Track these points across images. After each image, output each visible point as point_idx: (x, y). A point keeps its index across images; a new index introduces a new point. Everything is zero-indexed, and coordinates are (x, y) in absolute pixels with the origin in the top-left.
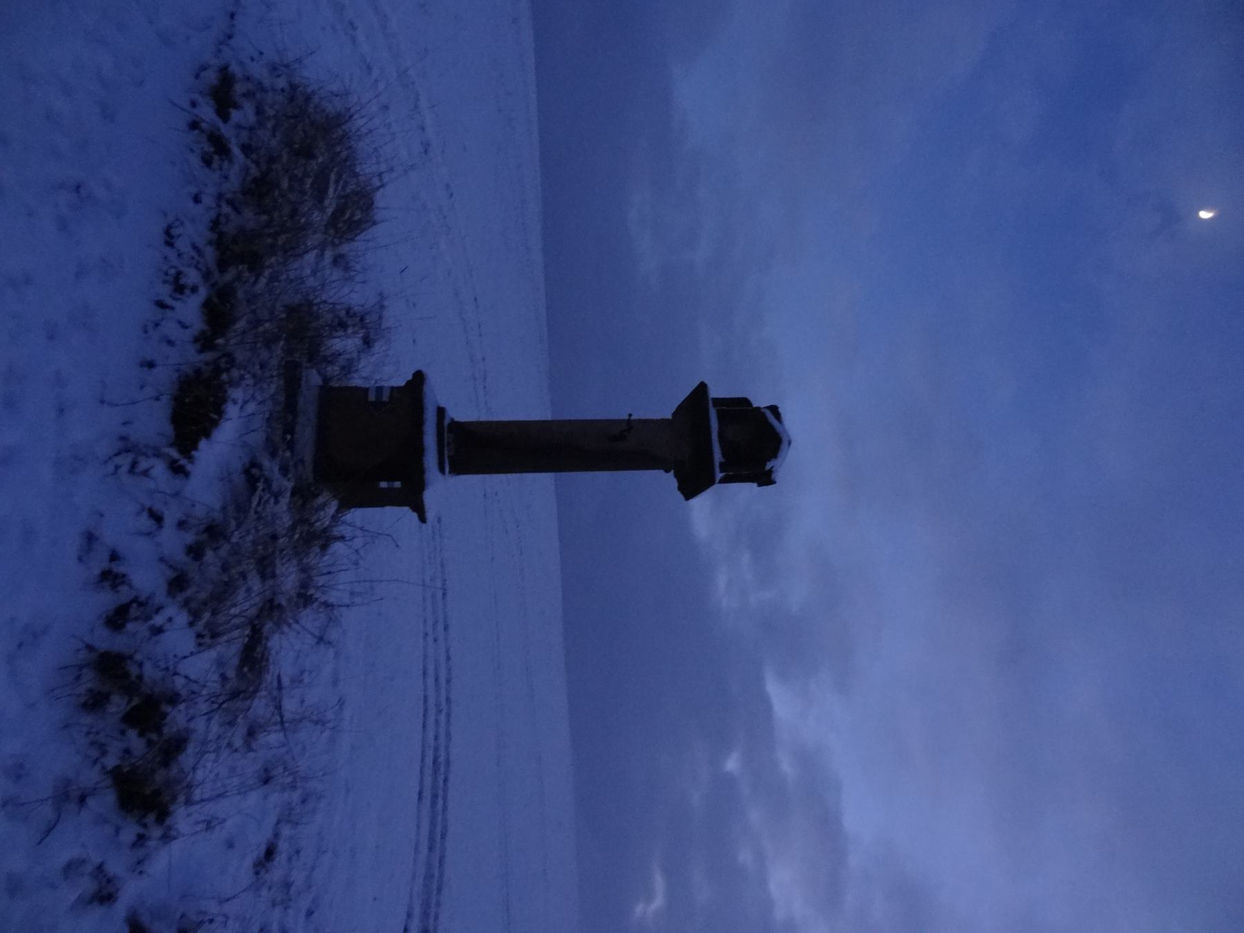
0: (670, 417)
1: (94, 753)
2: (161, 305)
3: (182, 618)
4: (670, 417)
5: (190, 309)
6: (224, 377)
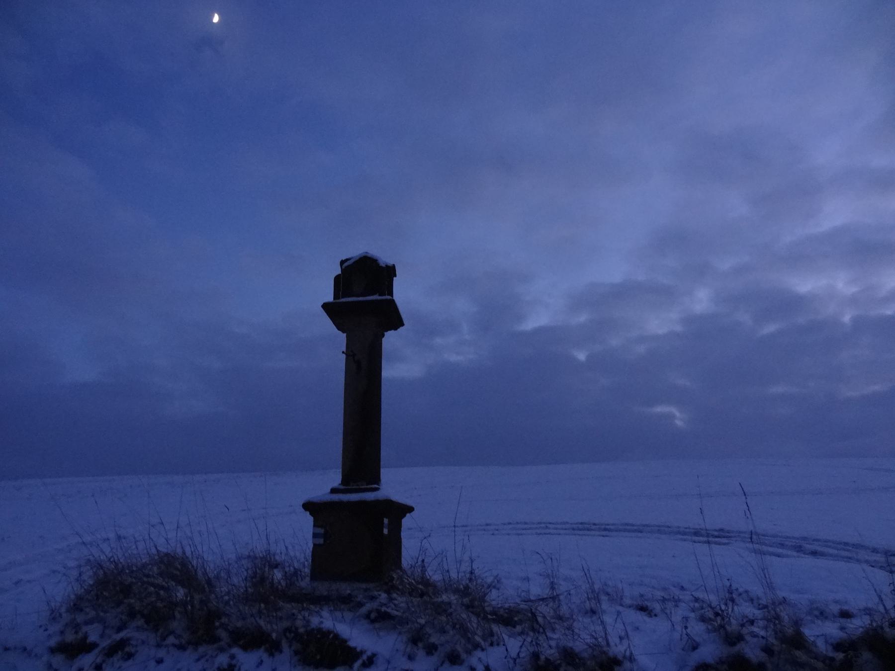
0: (345, 335)
3: (479, 653)
4: (345, 335)
6: (301, 630)
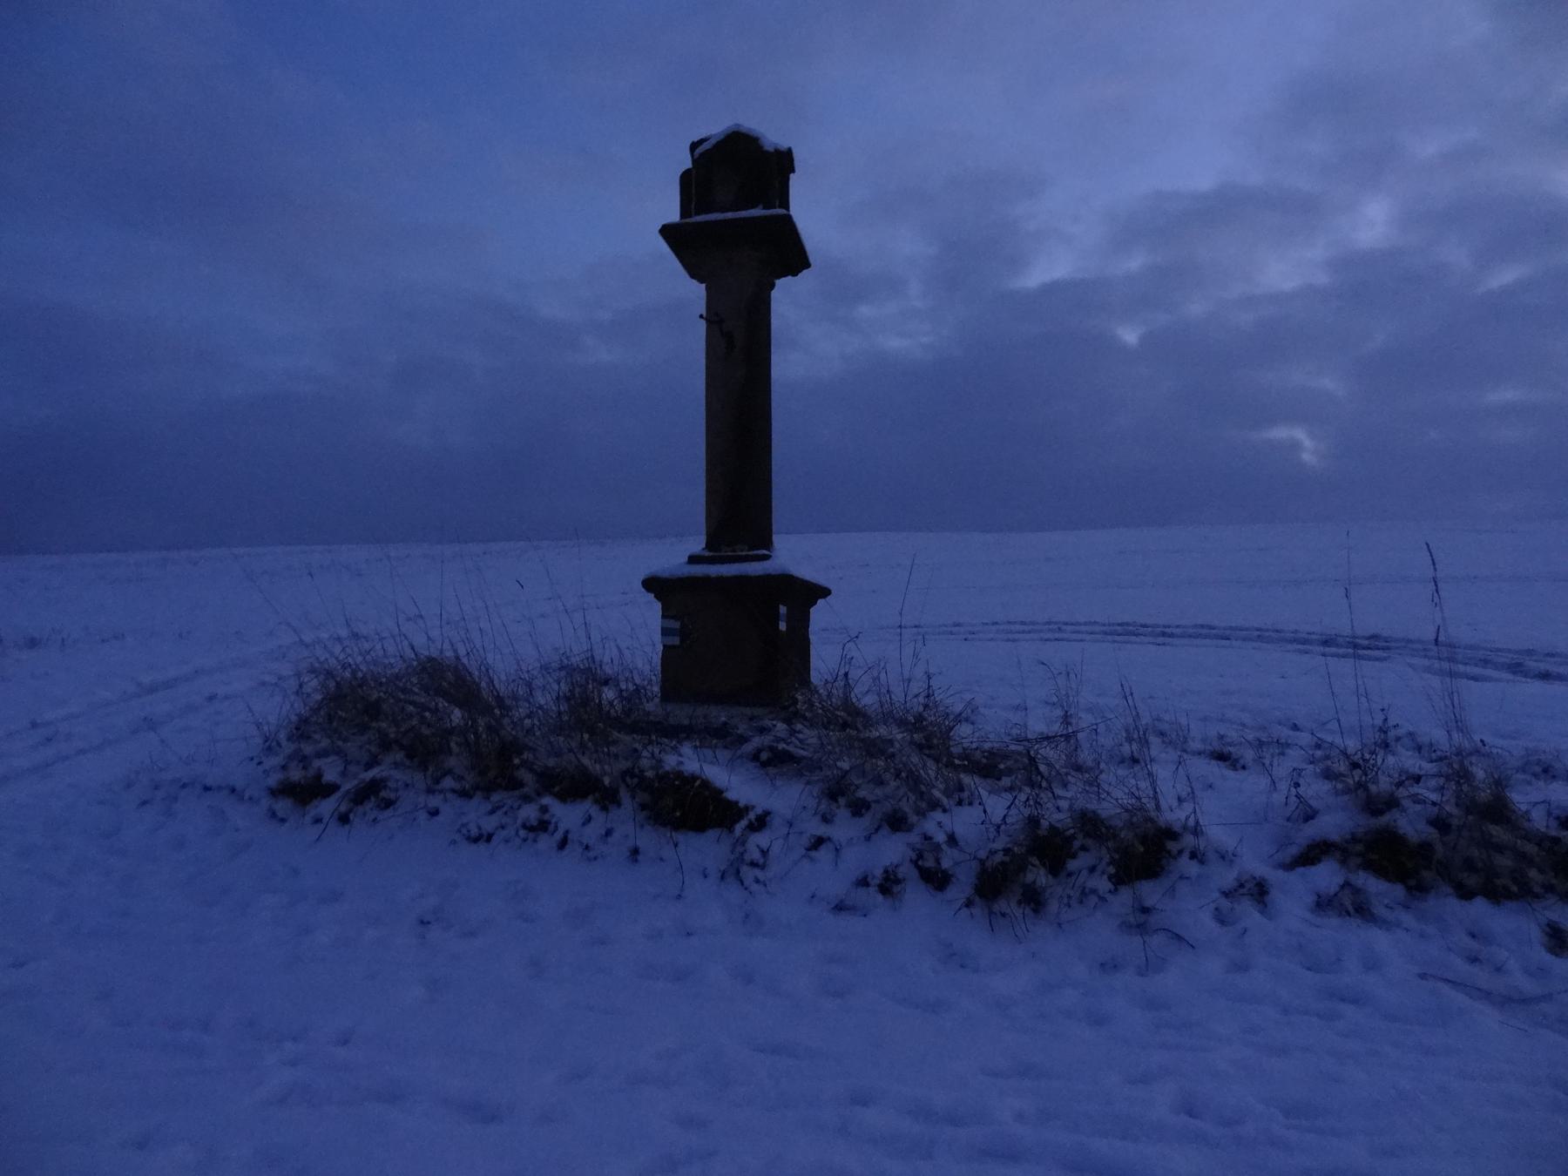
1: (1093, 899)
2: (563, 844)
5: (567, 815)
6: (650, 774)
